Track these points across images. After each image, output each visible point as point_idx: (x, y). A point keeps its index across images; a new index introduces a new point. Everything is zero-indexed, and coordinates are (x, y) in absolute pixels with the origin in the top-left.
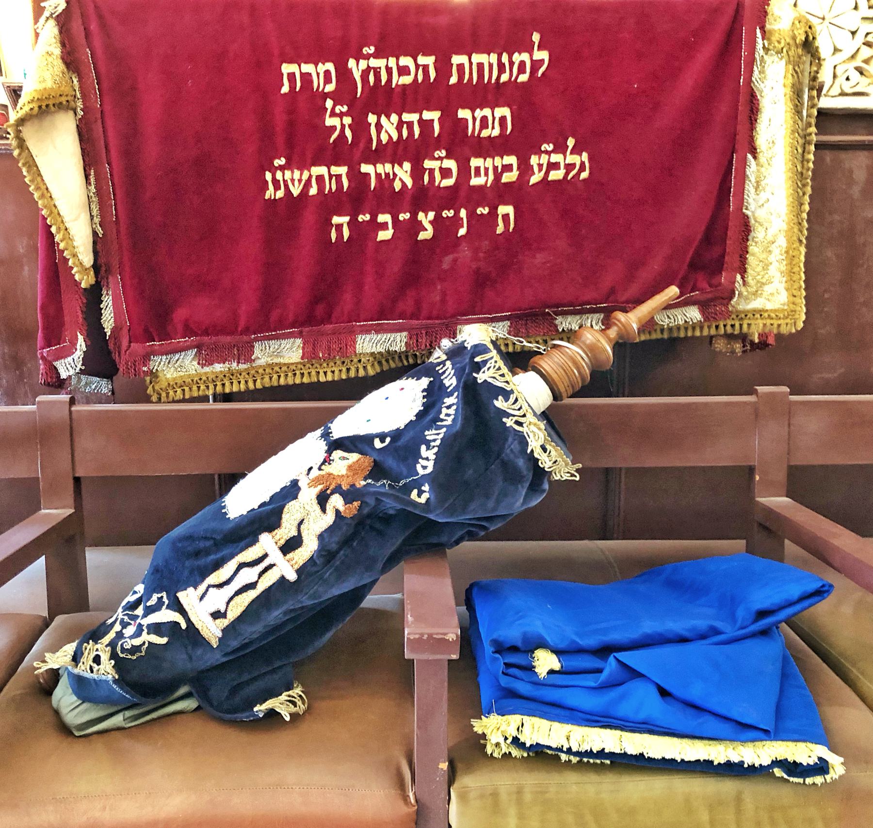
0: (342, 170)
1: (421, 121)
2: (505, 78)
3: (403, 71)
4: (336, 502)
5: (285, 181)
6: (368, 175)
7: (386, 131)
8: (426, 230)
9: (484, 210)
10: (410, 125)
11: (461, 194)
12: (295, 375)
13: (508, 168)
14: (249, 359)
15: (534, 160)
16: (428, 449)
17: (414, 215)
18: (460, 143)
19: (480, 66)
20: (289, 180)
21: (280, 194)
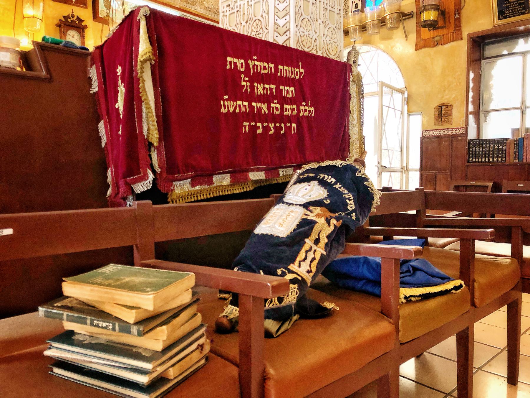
0: (246, 104)
1: (270, 88)
2: (292, 76)
3: (265, 68)
4: (333, 221)
5: (228, 106)
11: (282, 118)
13: (294, 109)
14: (211, 182)
15: (301, 108)
16: (350, 200)
18: (283, 101)
19: (286, 70)
20: (229, 106)
21: (226, 111)
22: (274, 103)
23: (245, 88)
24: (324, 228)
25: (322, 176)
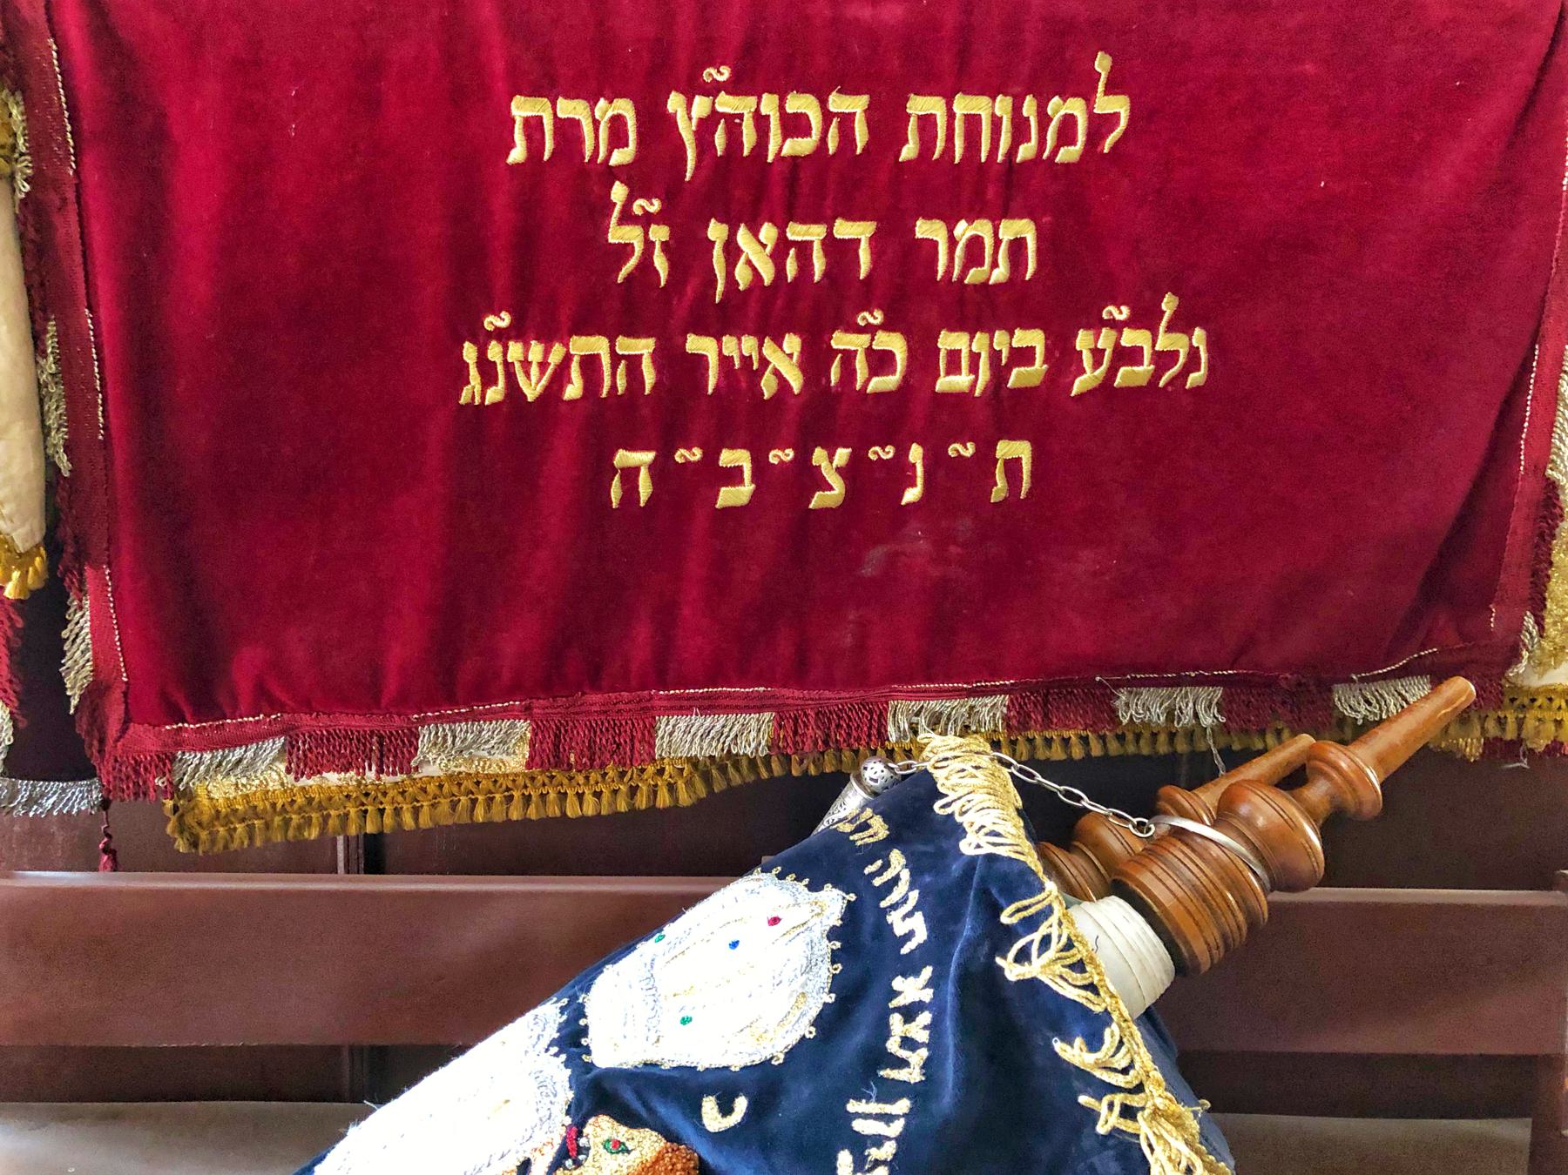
0: (644, 347)
1: (830, 243)
2: (1026, 151)
3: (795, 125)
6: (701, 360)
7: (749, 262)
8: (831, 488)
10: (804, 248)
11: (916, 410)
13: (1023, 356)
14: (398, 752)
19: (972, 121)
20: (516, 365)
21: (495, 394)
23: (633, 262)
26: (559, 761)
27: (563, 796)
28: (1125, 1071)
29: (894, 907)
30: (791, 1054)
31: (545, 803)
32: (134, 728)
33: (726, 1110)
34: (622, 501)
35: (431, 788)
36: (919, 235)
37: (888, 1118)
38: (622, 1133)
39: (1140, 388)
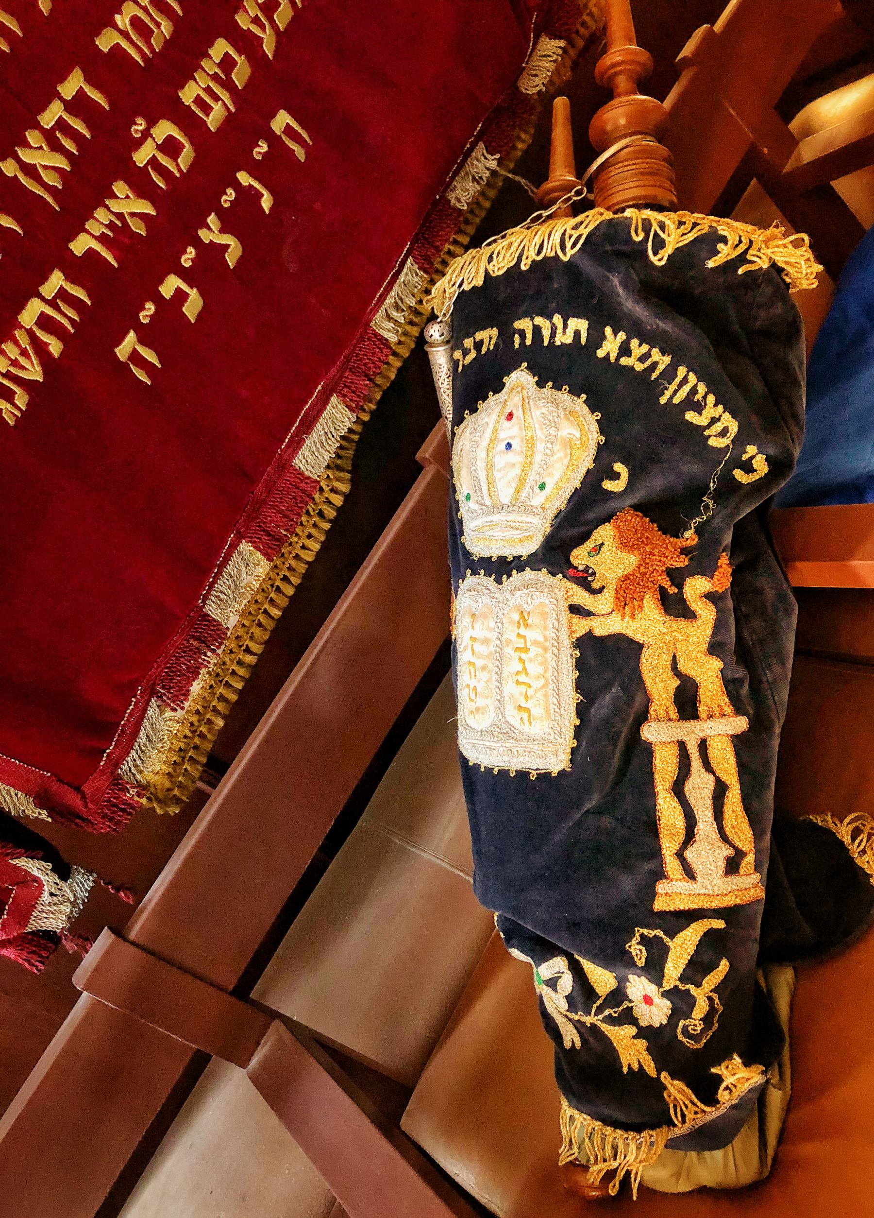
0: (56, 281)
1: (71, 106)
4: (696, 587)
6: (91, 253)
7: (46, 167)
8: (228, 246)
9: (262, 147)
10: (61, 124)
11: (220, 153)
12: (278, 589)
13: (227, 63)
14: (213, 632)
15: (243, 21)
16: (699, 408)
17: (197, 243)
21: (21, 399)
22: (138, 144)
24: (680, 646)
25: (524, 324)
26: (281, 541)
27: (297, 557)
28: (740, 242)
29: (553, 335)
30: (602, 432)
31: (294, 570)
32: (87, 788)
33: (616, 476)
34: (150, 376)
35: (241, 632)
36: (106, 50)
37: (685, 381)
38: (590, 544)
39: (293, 18)
